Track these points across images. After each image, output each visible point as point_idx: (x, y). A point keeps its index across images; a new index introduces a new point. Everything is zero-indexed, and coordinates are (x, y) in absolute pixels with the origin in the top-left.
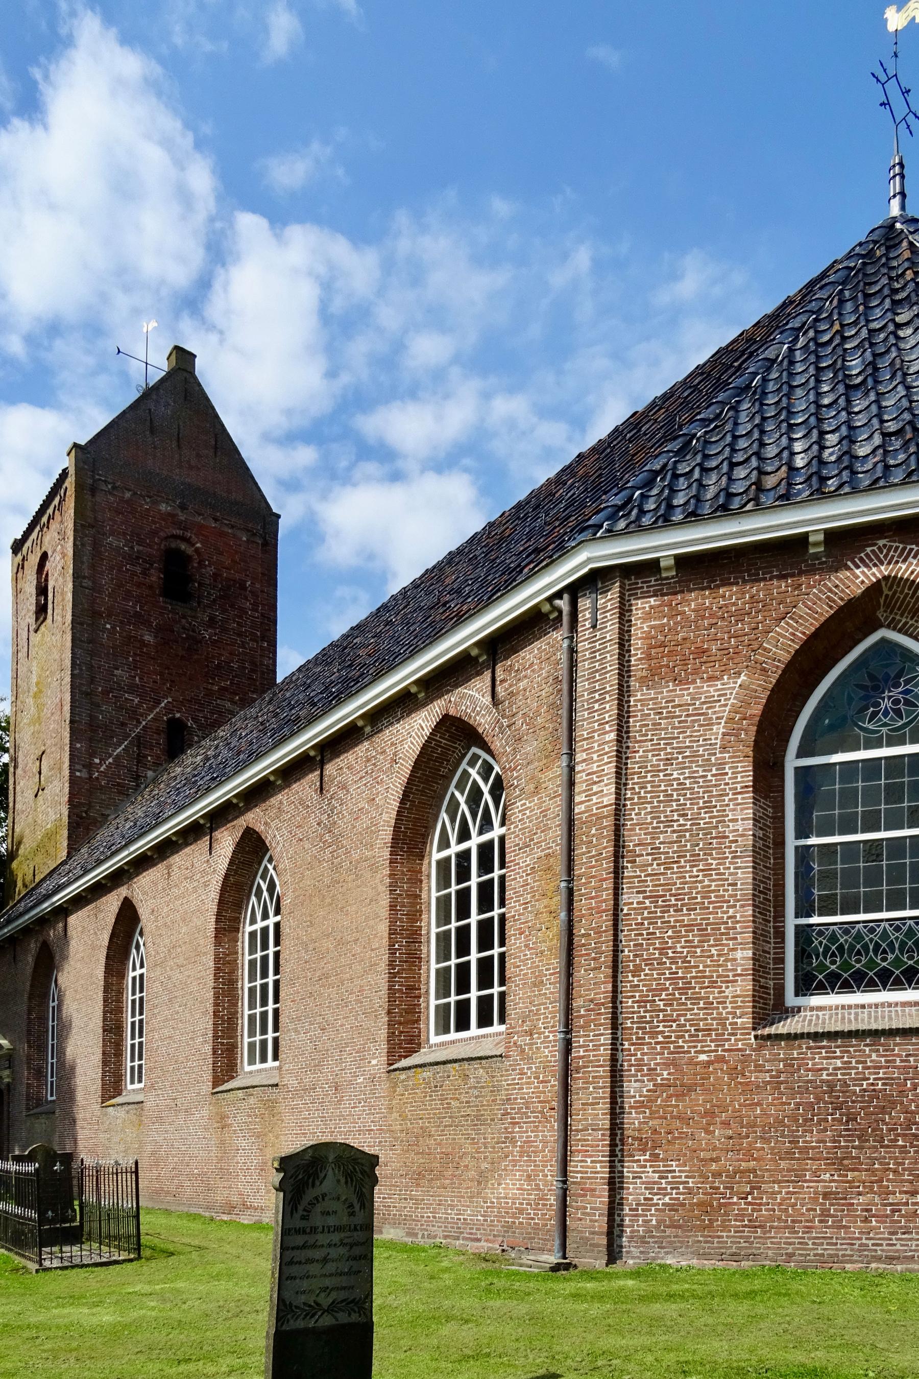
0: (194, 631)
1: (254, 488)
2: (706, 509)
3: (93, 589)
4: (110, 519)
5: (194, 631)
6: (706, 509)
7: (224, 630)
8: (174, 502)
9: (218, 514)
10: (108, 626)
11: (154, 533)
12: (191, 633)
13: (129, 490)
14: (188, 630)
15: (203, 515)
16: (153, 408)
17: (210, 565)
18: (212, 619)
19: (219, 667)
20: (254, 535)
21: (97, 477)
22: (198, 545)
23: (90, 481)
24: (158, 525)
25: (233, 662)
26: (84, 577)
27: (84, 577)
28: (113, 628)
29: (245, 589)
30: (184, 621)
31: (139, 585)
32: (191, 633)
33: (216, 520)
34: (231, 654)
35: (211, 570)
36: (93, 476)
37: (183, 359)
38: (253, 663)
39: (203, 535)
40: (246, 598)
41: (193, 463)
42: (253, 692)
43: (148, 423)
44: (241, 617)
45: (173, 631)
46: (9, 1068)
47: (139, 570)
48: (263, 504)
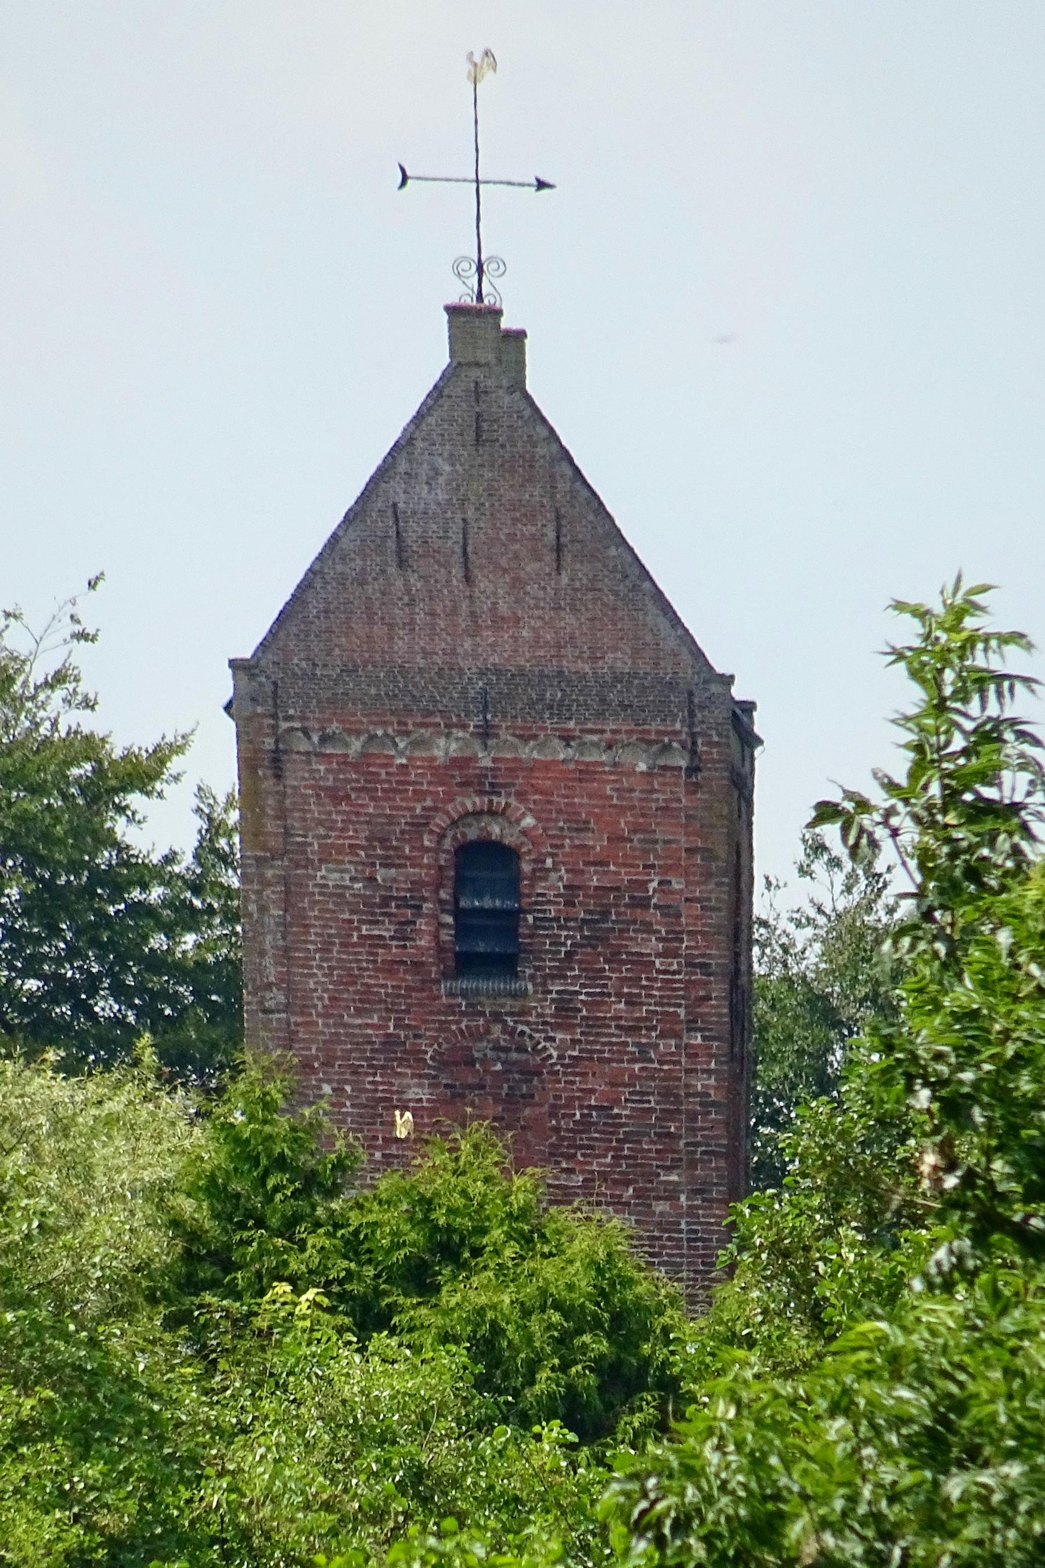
0: (521, 1049)
1: (663, 624)
2: (947, 781)
3: (287, 1008)
4: (320, 823)
5: (521, 1049)
6: (947, 781)
7: (594, 1024)
8: (464, 727)
9: (571, 724)
10: (327, 1089)
11: (420, 825)
12: (514, 1056)
13: (358, 733)
14: (506, 1050)
15: (535, 737)
16: (401, 499)
17: (555, 868)
18: (565, 1007)
19: (585, 1124)
20: (666, 748)
21: (284, 725)
22: (529, 821)
23: (269, 743)
24: (429, 803)
25: (617, 1102)
26: (269, 986)
27: (269, 986)
28: (338, 1091)
29: (643, 903)
30: (497, 1029)
31: (390, 968)
32: (514, 1056)
33: (567, 739)
34: (612, 1085)
35: (558, 880)
36: (275, 727)
37: (484, 344)
38: (666, 1094)
39: (538, 791)
40: (648, 928)
41: (503, 608)
42: (669, 1169)
43: (391, 544)
44: (635, 981)
45: (471, 1062)
46: (820, 1207)
47: (386, 930)
48: (686, 656)
